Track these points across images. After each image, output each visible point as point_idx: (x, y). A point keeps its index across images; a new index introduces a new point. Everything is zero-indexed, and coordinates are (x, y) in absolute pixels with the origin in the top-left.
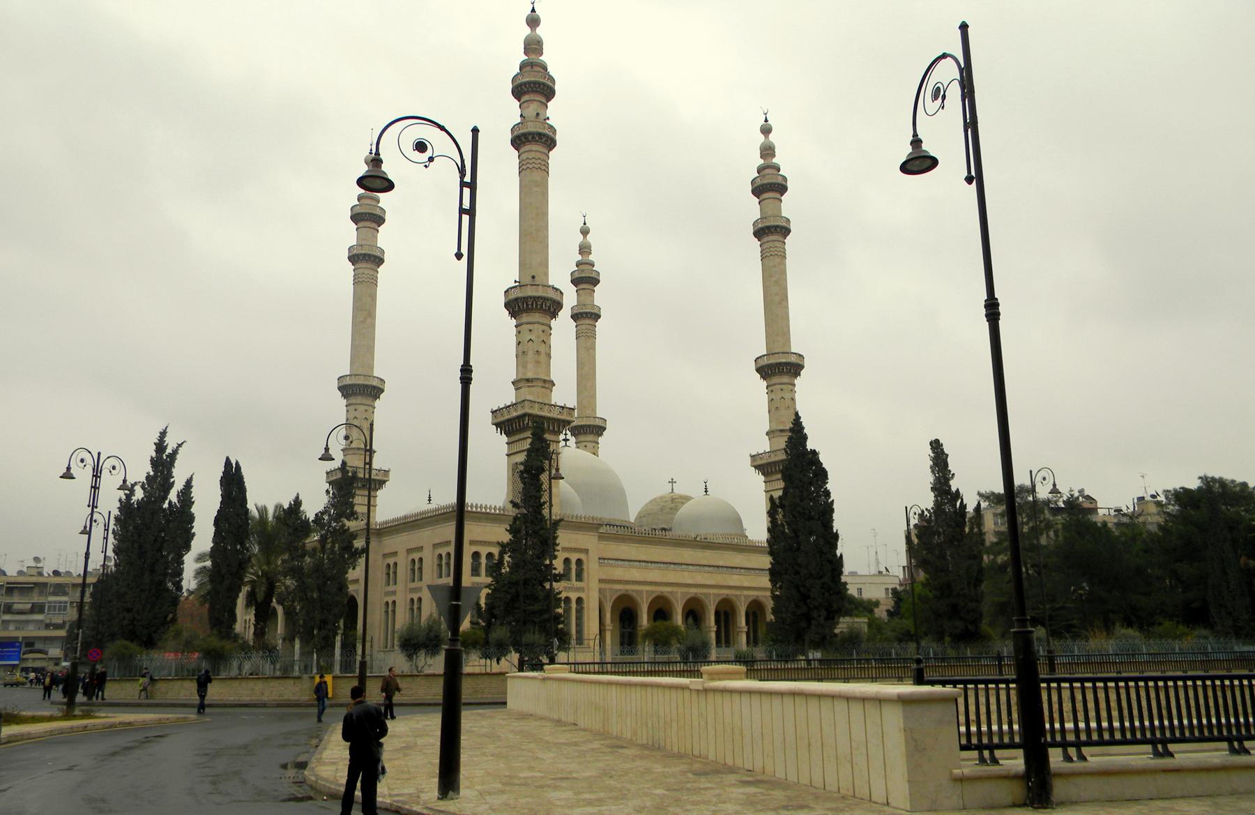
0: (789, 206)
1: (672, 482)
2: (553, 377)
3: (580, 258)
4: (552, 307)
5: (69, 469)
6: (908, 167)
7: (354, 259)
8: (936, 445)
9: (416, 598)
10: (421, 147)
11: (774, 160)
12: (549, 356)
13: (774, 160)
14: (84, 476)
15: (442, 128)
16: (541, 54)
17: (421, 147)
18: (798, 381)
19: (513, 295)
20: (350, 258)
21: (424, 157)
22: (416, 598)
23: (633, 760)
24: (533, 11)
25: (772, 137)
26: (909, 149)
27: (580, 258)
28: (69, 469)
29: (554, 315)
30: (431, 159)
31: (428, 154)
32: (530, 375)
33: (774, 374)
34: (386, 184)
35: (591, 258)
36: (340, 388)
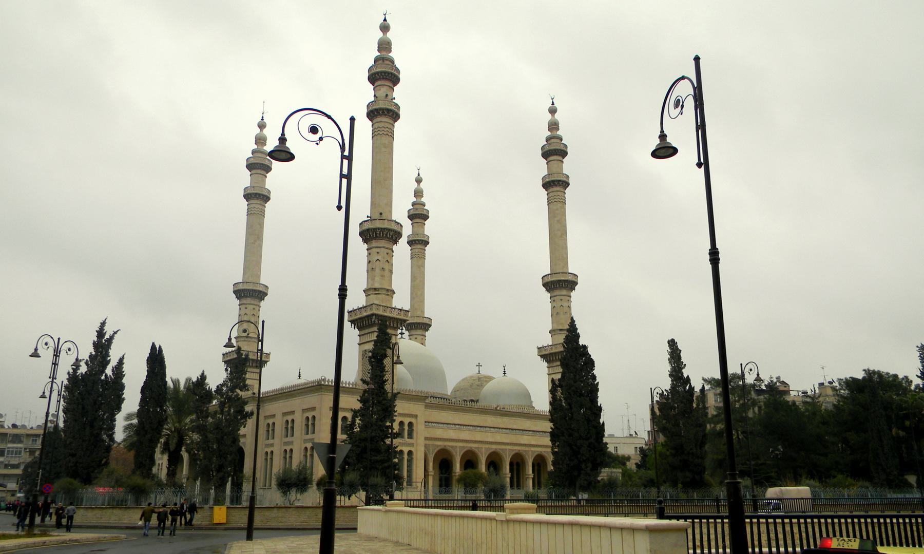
1: (479, 365)
2: (394, 288)
3: (414, 199)
4: (394, 236)
5: (36, 350)
7: (247, 197)
10: (314, 130)
11: (558, 133)
12: (391, 272)
13: (558, 133)
14: (47, 355)
15: (329, 117)
16: (390, 51)
17: (314, 130)
19: (367, 226)
20: (245, 196)
24: (385, 20)
25: (389, 35)
27: (414, 199)
28: (36, 350)
30: (321, 139)
31: (319, 135)
32: (377, 286)
35: (423, 200)
36: (544, 285)
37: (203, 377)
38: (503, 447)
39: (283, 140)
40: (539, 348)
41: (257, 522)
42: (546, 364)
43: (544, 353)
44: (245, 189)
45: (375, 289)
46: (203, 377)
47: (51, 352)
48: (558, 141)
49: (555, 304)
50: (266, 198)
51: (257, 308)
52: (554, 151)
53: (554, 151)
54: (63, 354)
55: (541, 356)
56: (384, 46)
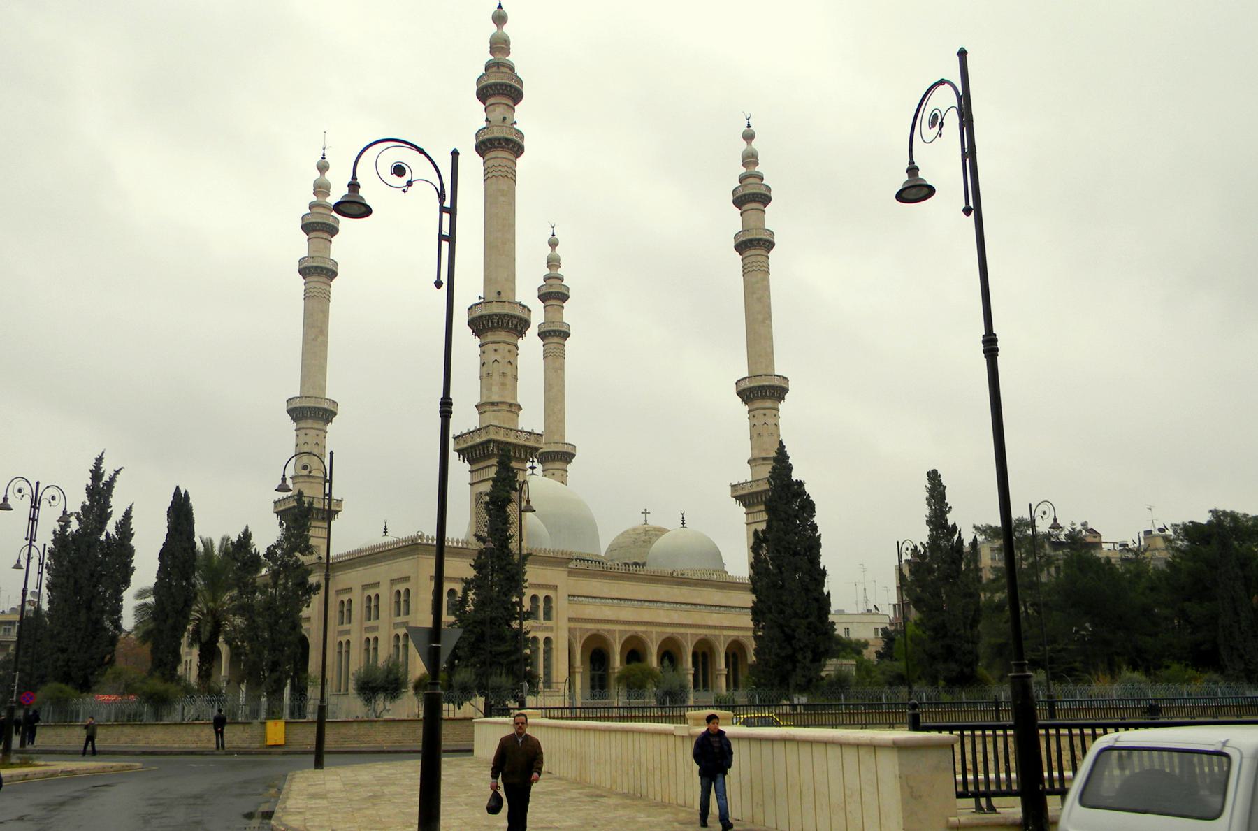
1: (646, 513)
2: (519, 401)
3: (547, 271)
4: (519, 325)
11: (757, 169)
12: (515, 378)
13: (757, 169)
15: (421, 151)
17: (399, 170)
19: (477, 312)
21: (402, 181)
27: (547, 271)
29: (521, 334)
30: (410, 183)
31: (407, 177)
35: (560, 271)
36: (739, 394)
37: (246, 536)
43: (741, 492)
45: (493, 404)
46: (246, 536)
47: (27, 502)
48: (758, 181)
54: (44, 505)
55: (736, 498)
56: (750, 159)
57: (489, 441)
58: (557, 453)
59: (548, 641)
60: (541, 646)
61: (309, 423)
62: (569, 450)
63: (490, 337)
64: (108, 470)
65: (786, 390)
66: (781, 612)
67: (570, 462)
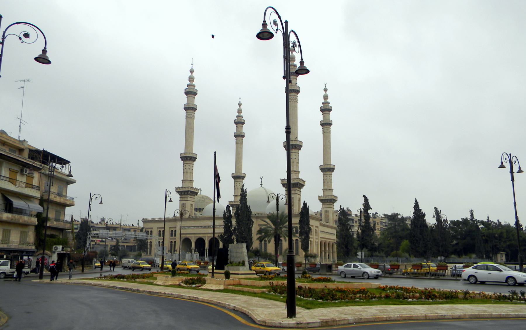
0: (197, 100)
1: (511, 165)
2: (299, 170)
3: (189, 83)
5: (502, 163)
6: (261, 36)
7: (186, 109)
8: (436, 209)
9: (173, 241)
12: (298, 163)
14: (507, 165)
16: (295, 61)
18: (300, 152)
22: (173, 241)
23: (138, 275)
26: (261, 28)
27: (189, 83)
28: (502, 163)
33: (187, 160)
34: (270, 35)
35: (194, 83)
36: (181, 158)
38: (204, 235)
39: (302, 62)
40: (319, 196)
41: (210, 223)
42: (321, 204)
44: (321, 107)
45: (295, 171)
49: (326, 178)
50: (195, 109)
51: (191, 165)
52: (239, 123)
53: (239, 123)
57: (189, 191)
58: (189, 157)
59: (151, 242)
60: (149, 244)
61: (190, 95)
62: (194, 156)
63: (189, 95)
64: (244, 188)
65: (301, 146)
66: (424, 240)
67: (194, 161)
